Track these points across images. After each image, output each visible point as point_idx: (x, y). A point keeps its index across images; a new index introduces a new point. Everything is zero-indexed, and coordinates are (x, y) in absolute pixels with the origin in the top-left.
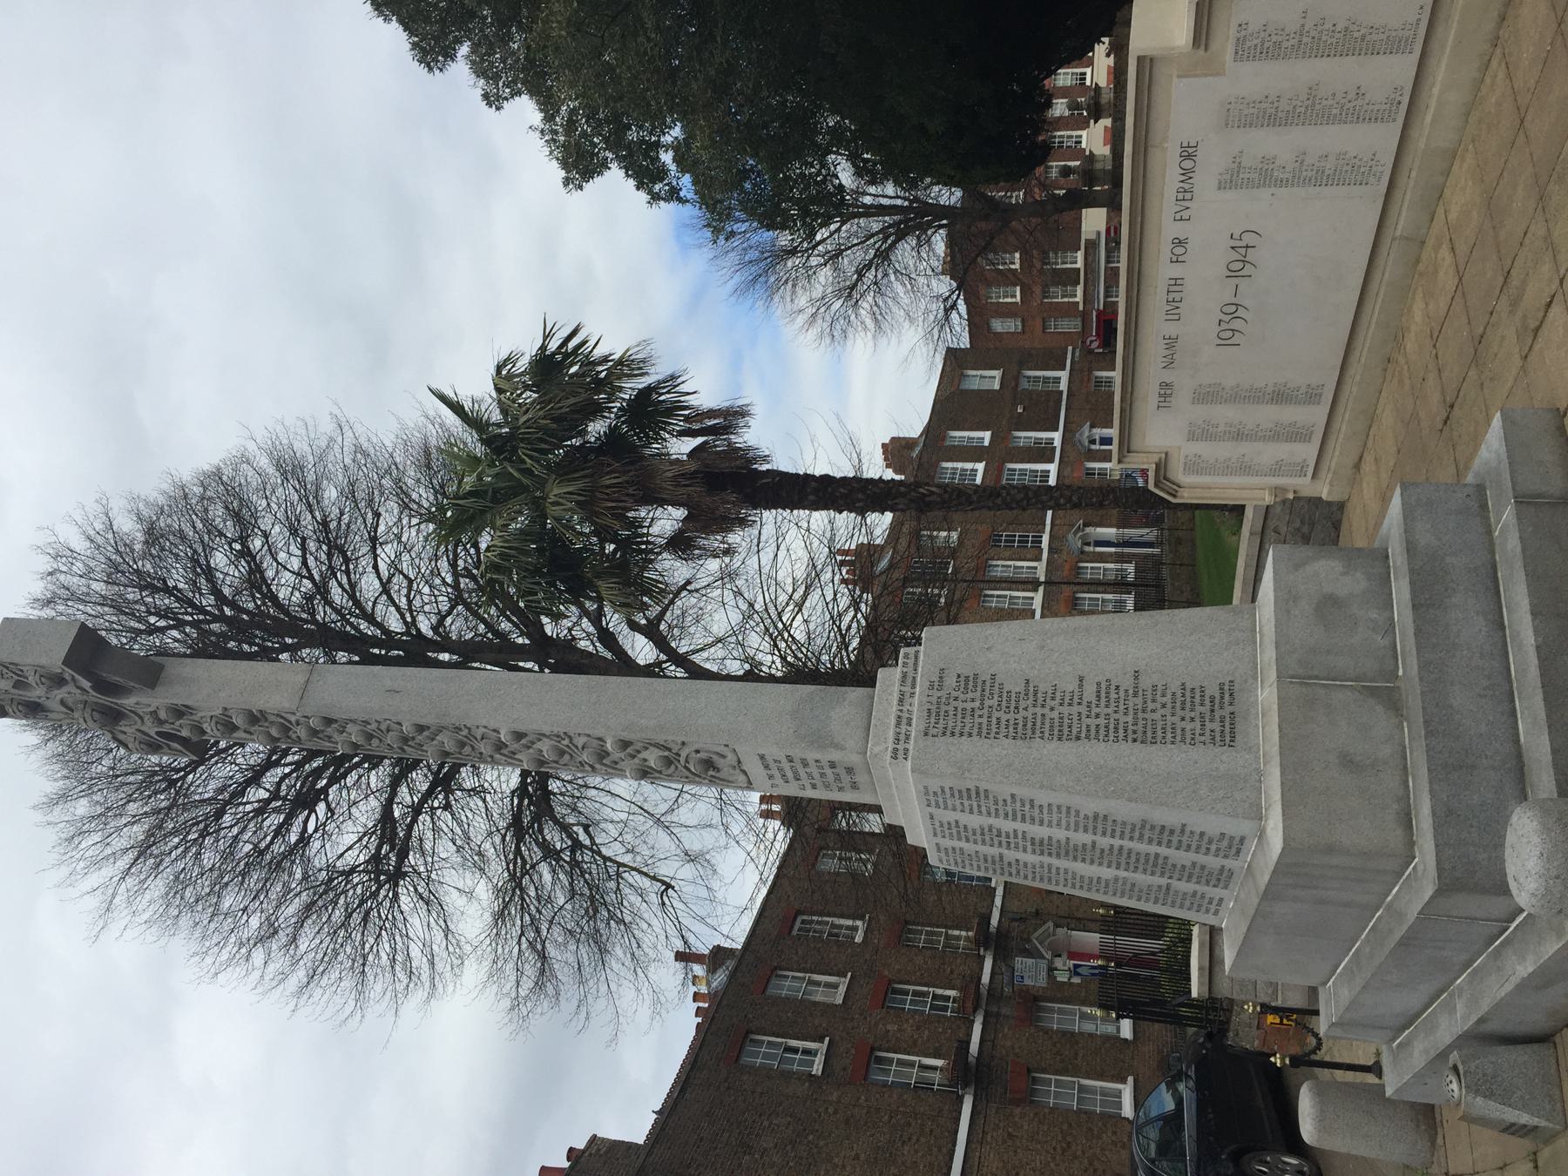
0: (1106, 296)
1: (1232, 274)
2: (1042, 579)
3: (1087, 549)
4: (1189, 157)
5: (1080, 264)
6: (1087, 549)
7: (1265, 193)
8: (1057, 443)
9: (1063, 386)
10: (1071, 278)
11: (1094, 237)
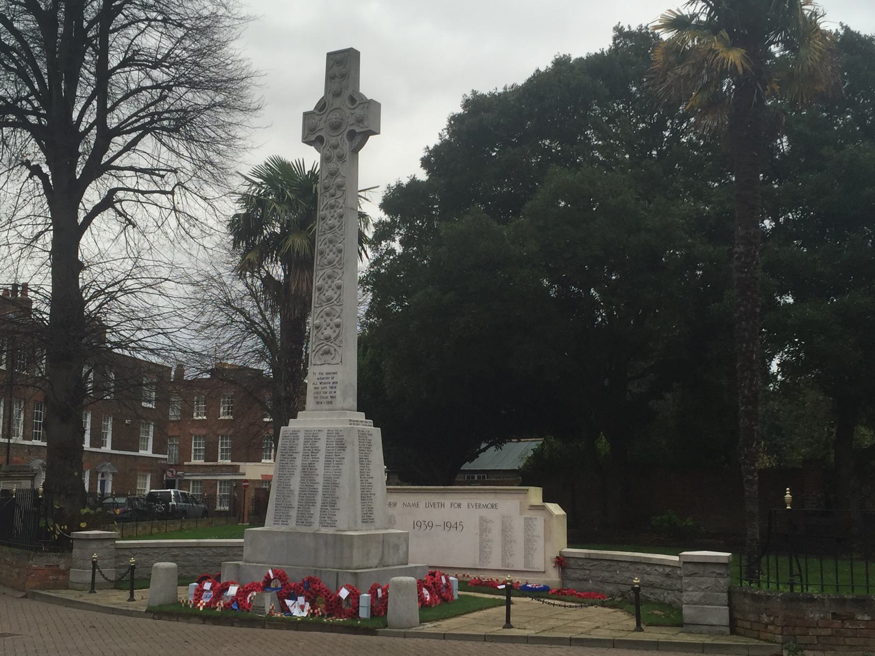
0: (194, 481)
1: (445, 524)
2: (12, 441)
3: (100, 475)
4: (492, 507)
5: (220, 462)
6: (100, 475)
7: (478, 531)
8: (103, 449)
9: (142, 453)
10: (210, 454)
11: (241, 471)
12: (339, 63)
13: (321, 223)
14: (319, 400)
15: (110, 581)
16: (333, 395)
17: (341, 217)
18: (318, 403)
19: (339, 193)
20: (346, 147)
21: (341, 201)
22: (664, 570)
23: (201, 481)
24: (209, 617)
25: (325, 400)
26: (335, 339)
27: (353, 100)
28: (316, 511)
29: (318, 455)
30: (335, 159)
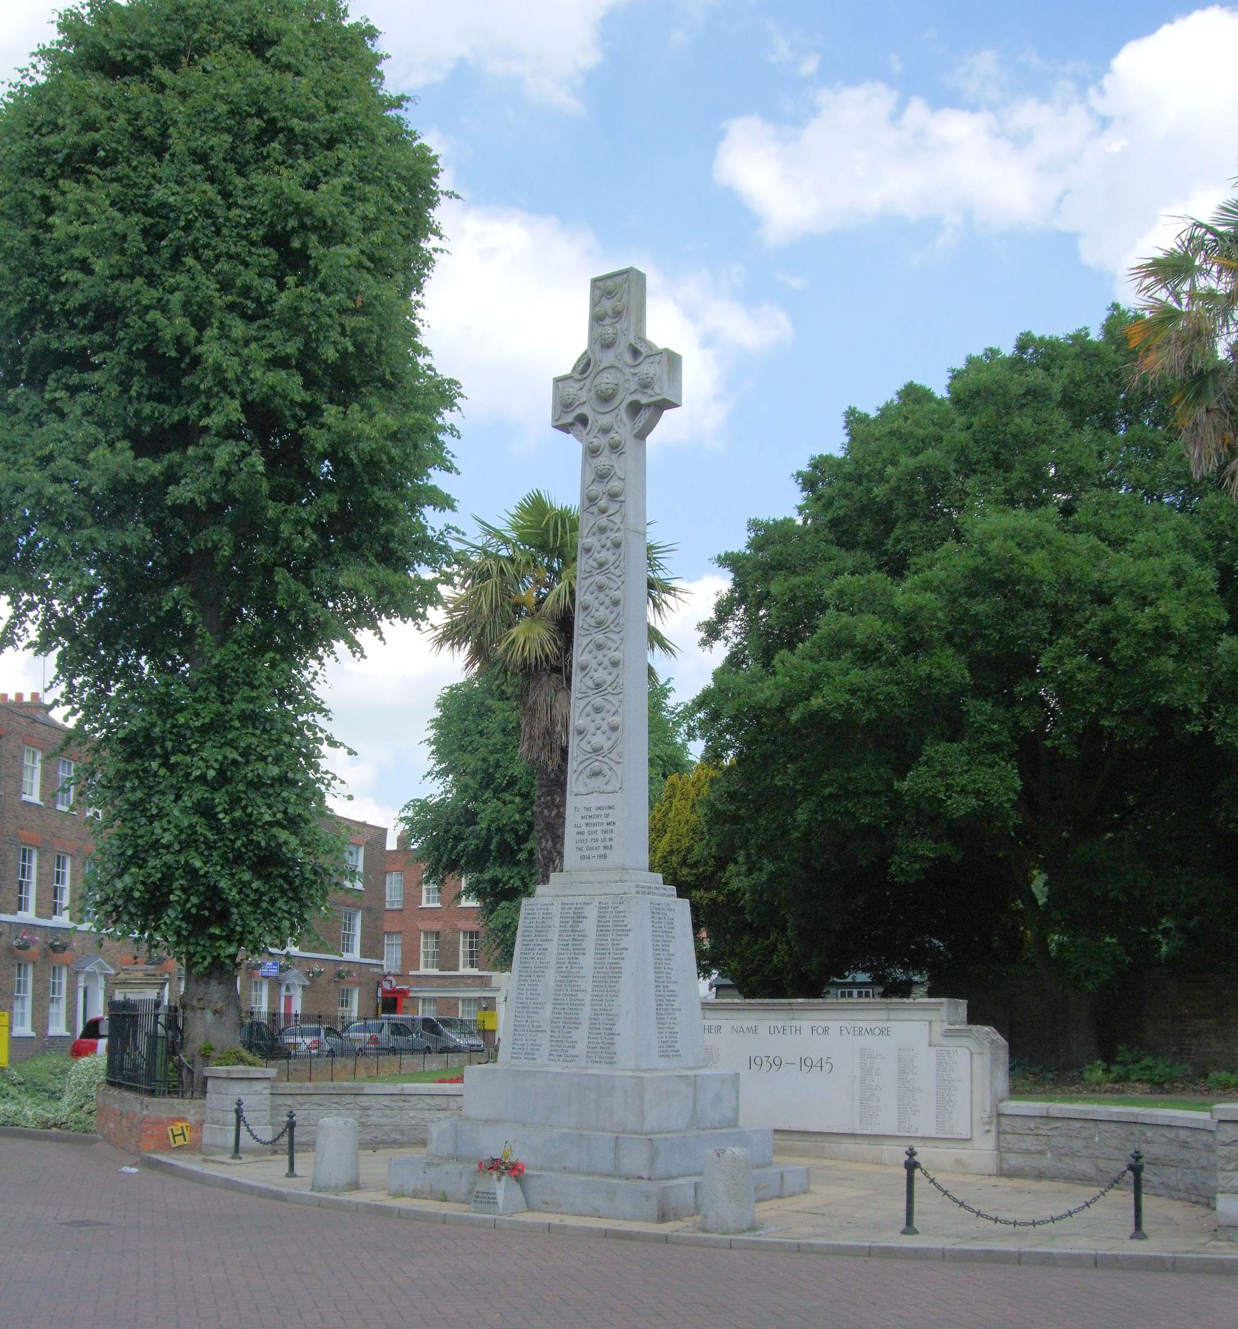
3: (283, 988)
4: (882, 1032)
6: (283, 988)
9: (347, 956)
12: (609, 294)
13: (585, 557)
14: (585, 853)
15: (264, 1143)
16: (609, 844)
17: (617, 545)
18: (583, 857)
19: (613, 508)
20: (624, 430)
21: (617, 519)
22: (1177, 1136)
23: (434, 1000)
24: (49, 1130)
25: (594, 853)
26: (611, 750)
27: (635, 352)
28: (581, 1035)
29: (584, 945)
30: (606, 452)
